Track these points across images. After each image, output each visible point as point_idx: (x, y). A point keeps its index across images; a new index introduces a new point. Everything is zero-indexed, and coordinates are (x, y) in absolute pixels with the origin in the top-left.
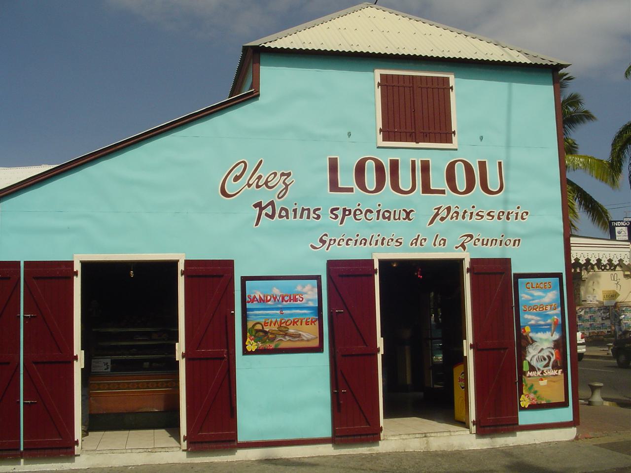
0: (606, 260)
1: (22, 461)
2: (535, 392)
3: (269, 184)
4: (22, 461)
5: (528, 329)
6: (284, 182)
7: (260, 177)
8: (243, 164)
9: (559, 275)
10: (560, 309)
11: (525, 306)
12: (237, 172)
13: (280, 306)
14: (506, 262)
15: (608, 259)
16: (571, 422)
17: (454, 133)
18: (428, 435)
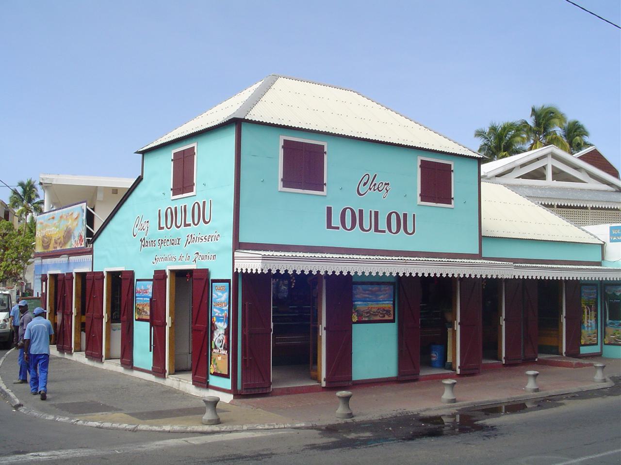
0: (323, 271)
1: (66, 353)
2: (216, 364)
3: (379, 189)
4: (66, 353)
5: (215, 319)
6: (386, 189)
7: (375, 184)
8: (196, 204)
9: (228, 281)
10: (228, 306)
11: (215, 303)
12: (365, 180)
13: (143, 296)
14: (206, 272)
15: (317, 270)
16: (229, 390)
17: (325, 153)
18: (181, 380)
